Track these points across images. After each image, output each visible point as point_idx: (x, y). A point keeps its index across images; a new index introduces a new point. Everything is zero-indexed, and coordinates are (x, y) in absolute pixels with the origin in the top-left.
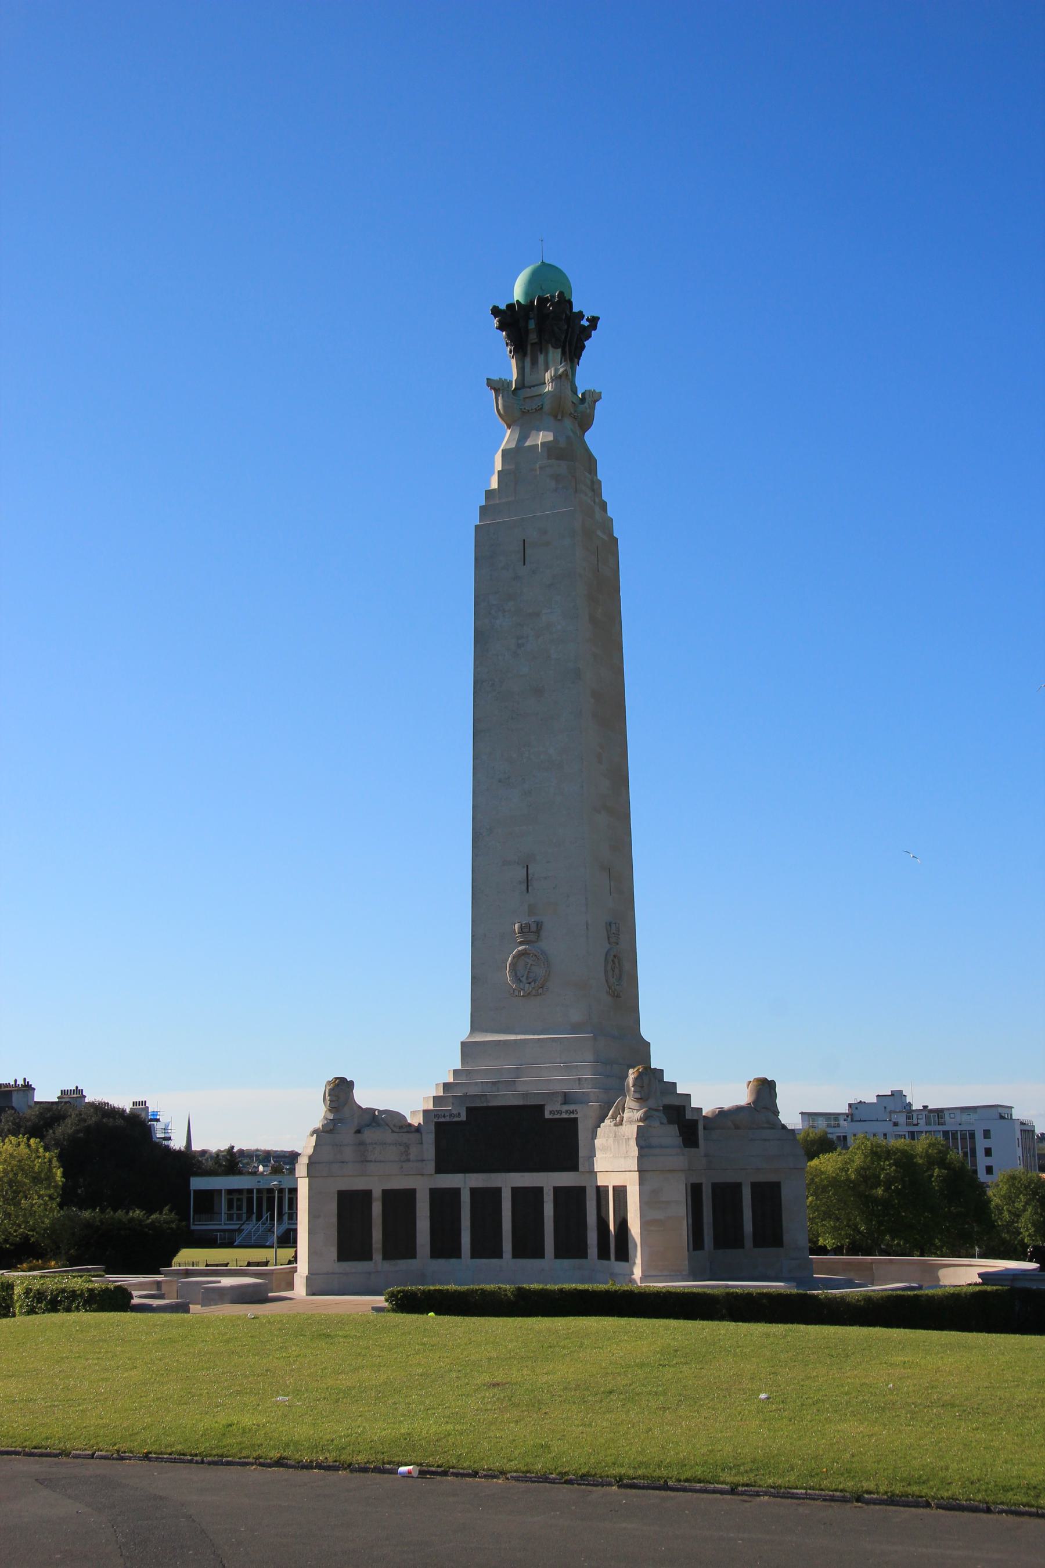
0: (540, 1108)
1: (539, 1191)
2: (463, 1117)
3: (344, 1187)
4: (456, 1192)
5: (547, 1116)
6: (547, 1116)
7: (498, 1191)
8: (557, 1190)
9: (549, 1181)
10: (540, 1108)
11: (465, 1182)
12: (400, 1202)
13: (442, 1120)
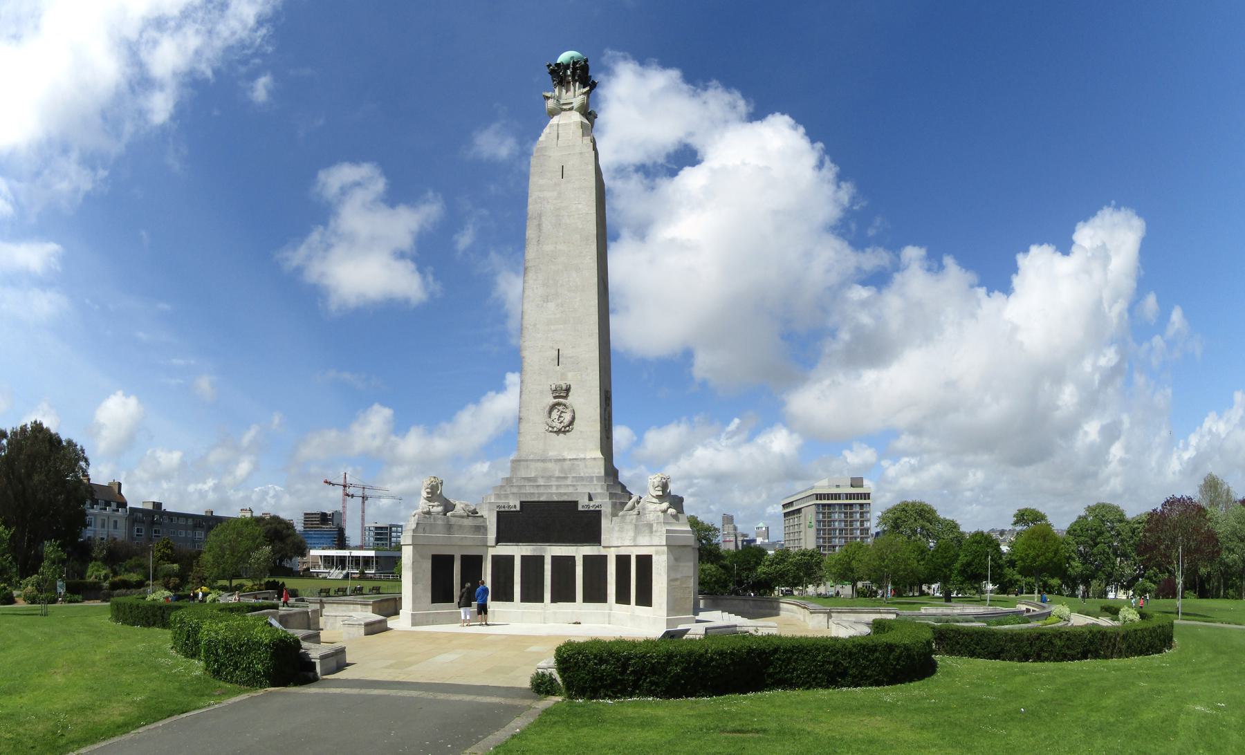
0: (576, 503)
1: (572, 559)
3: (524, 554)
4: (510, 559)
5: (580, 508)
6: (580, 508)
7: (512, 558)
8: (585, 557)
9: (579, 552)
10: (576, 503)
11: (518, 551)
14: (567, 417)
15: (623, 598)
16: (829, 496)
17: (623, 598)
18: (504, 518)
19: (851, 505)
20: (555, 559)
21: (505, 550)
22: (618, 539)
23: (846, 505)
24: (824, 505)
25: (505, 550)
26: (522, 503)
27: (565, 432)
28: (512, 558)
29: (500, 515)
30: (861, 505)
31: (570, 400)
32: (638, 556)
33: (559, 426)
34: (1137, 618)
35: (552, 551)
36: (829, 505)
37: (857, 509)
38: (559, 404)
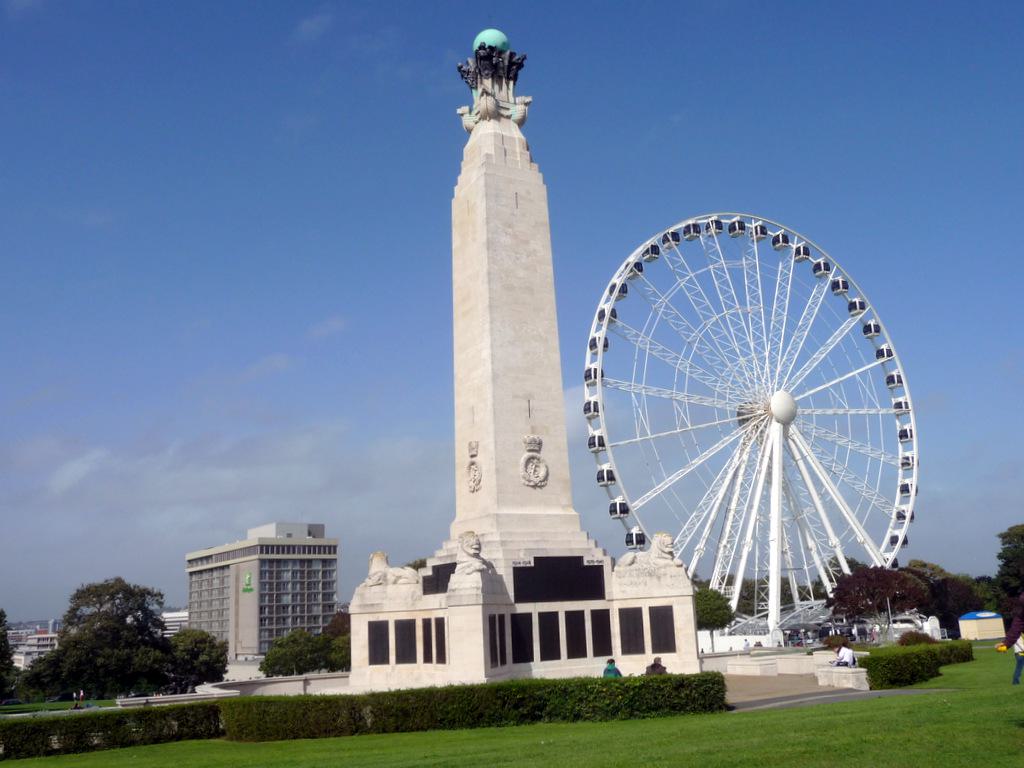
0: (580, 559)
1: (555, 615)
2: (532, 564)
5: (586, 564)
6: (586, 564)
9: (587, 606)
10: (580, 559)
11: (534, 609)
12: (406, 628)
13: (518, 565)
14: (542, 473)
15: (428, 659)
16: (280, 549)
17: (428, 659)
18: (520, 573)
19: (310, 561)
20: (542, 615)
21: (522, 608)
22: (623, 590)
23: (302, 561)
24: (271, 561)
25: (522, 608)
26: (536, 559)
27: (541, 487)
28: (581, 613)
29: (516, 570)
30: (324, 561)
31: (542, 455)
32: (651, 609)
33: (537, 480)
34: (868, 627)
35: (561, 608)
36: (279, 561)
37: (319, 567)
38: (533, 458)
